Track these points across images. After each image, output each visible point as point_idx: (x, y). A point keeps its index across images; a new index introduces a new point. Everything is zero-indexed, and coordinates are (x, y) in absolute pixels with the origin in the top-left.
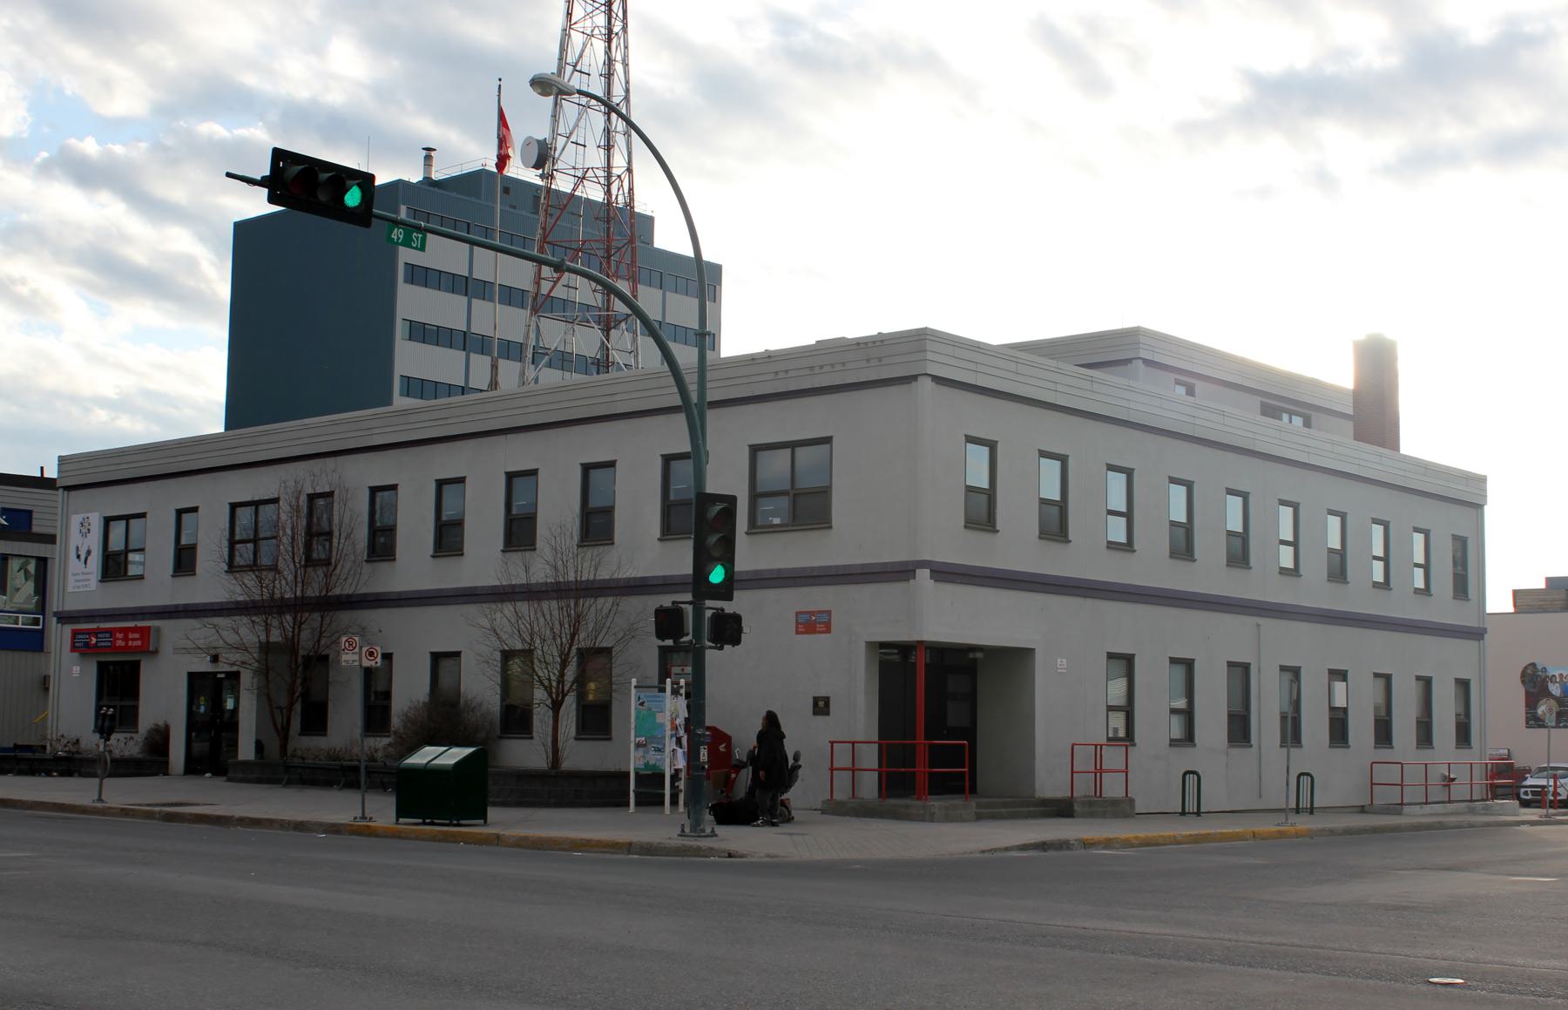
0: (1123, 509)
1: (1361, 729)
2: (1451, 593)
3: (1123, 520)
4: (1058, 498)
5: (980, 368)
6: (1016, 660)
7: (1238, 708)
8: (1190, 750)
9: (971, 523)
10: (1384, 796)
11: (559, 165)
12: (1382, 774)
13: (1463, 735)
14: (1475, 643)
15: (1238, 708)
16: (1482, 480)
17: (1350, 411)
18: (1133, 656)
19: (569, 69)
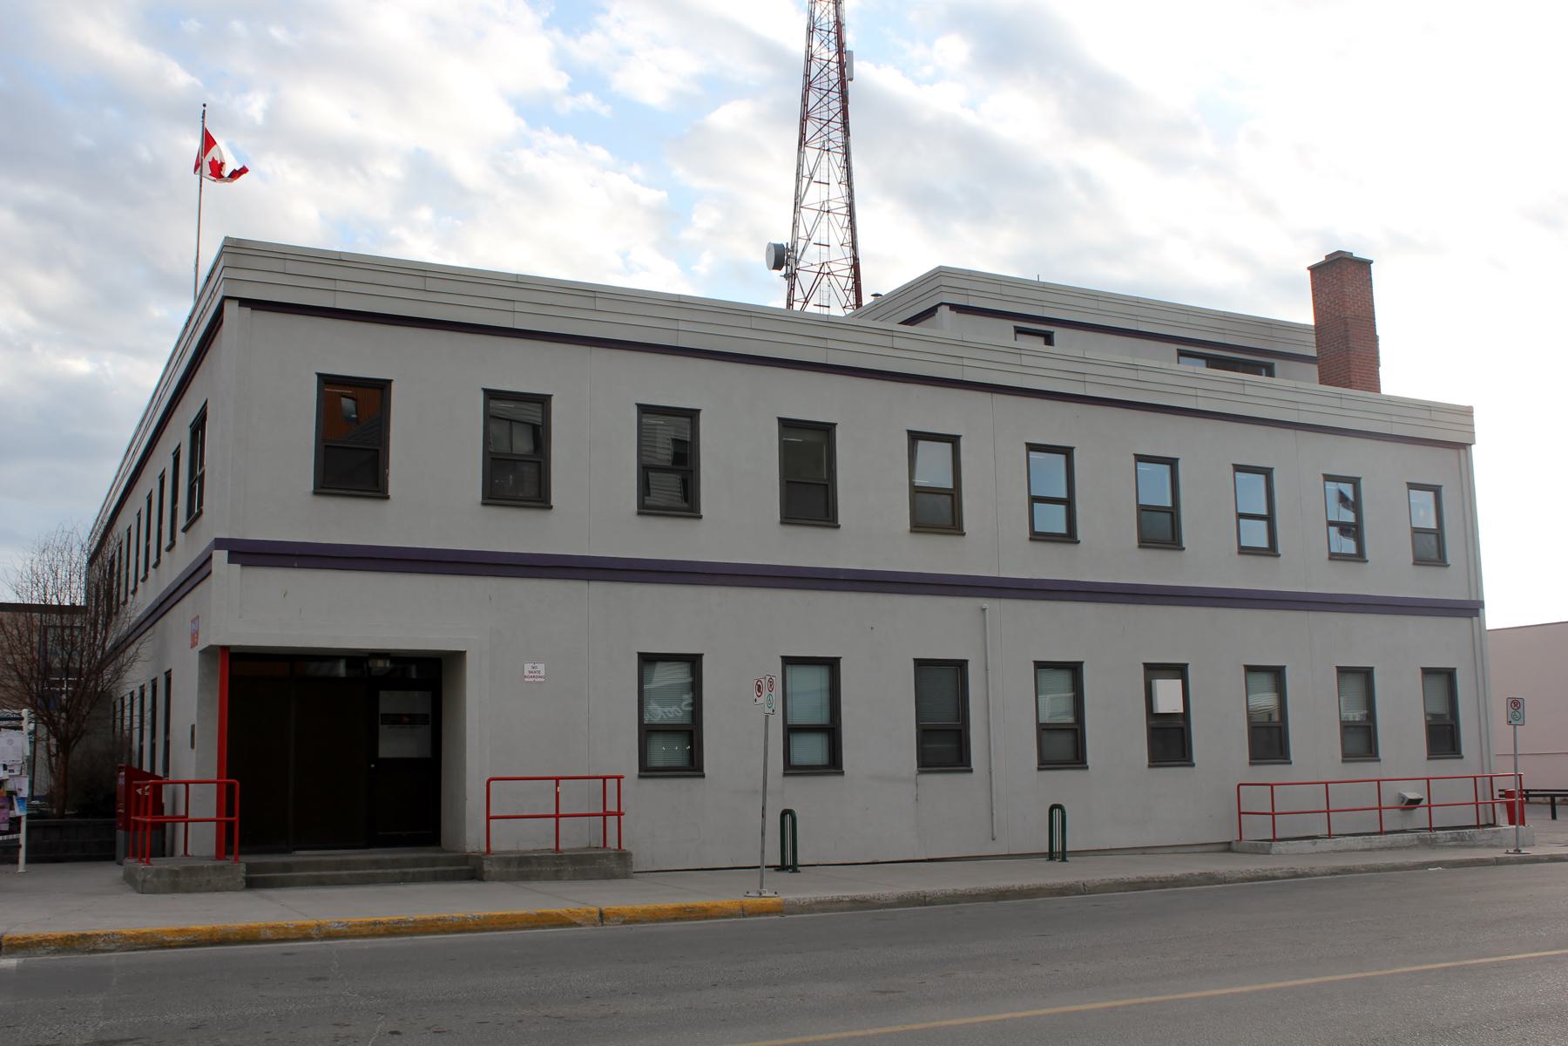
0: (1264, 512)
1: (1220, 737)
2: (309, 483)
3: (1061, 509)
4: (1169, 504)
6: (430, 677)
7: (1440, 708)
8: (837, 779)
9: (1147, 541)
10: (1257, 829)
11: (801, 264)
12: (1256, 799)
13: (1443, 737)
15: (1440, 708)
16: (1467, 412)
17: (1313, 353)
18: (700, 656)
19: (805, 181)
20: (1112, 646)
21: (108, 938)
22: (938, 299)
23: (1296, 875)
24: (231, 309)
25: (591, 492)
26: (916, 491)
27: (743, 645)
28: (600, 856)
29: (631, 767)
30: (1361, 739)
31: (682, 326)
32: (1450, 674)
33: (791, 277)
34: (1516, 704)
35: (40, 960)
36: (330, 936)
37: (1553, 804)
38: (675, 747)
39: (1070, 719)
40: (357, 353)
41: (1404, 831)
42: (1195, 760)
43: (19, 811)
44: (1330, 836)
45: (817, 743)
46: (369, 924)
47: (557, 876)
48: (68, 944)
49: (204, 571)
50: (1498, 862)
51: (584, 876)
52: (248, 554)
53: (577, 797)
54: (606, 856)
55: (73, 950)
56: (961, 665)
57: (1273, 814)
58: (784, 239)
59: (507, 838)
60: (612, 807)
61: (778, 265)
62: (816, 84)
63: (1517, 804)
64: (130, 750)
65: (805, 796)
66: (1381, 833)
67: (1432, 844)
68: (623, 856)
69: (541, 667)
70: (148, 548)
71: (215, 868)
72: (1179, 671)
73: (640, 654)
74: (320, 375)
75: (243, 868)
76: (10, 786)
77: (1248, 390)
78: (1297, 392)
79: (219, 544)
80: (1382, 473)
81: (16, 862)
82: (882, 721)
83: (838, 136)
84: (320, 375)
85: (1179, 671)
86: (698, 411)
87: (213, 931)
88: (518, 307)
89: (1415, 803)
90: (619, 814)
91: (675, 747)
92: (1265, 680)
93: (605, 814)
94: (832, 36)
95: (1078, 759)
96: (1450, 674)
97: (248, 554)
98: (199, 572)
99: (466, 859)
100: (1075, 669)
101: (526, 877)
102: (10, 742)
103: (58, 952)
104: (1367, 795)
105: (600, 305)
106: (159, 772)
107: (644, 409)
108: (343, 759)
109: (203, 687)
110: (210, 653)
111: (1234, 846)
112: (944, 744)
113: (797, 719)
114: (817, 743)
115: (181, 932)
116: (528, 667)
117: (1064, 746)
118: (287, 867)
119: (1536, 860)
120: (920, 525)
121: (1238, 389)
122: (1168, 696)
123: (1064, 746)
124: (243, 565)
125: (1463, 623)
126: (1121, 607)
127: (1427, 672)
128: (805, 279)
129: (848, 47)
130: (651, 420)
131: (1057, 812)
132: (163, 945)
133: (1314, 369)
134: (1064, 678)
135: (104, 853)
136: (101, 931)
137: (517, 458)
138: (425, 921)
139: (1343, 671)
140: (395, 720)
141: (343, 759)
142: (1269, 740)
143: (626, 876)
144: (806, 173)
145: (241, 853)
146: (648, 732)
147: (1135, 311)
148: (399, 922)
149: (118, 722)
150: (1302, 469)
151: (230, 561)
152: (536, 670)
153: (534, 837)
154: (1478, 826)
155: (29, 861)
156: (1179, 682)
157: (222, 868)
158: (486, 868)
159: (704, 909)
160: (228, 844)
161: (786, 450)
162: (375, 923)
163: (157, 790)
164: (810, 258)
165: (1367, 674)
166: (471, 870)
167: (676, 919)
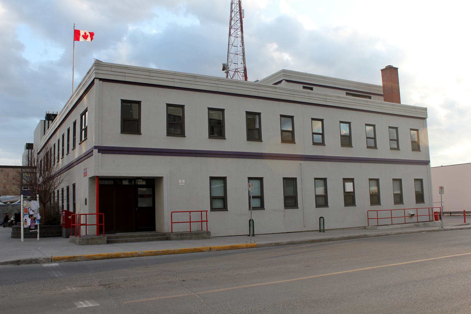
1: (363, 199)
3: (373, 140)
5: (127, 75)
6: (153, 183)
7: (419, 190)
11: (230, 69)
13: (420, 198)
14: (425, 166)
16: (426, 109)
18: (263, 178)
19: (231, 46)
20: (334, 173)
21: (80, 257)
22: (288, 78)
23: (387, 235)
24: (97, 81)
25: (196, 133)
26: (282, 131)
27: (238, 175)
28: (202, 233)
29: (209, 209)
30: (399, 199)
31: (220, 86)
32: (421, 180)
33: (227, 73)
34: (441, 188)
35: (63, 263)
36: (139, 256)
37: (465, 216)
38: (220, 202)
39: (323, 194)
40: (132, 94)
41: (410, 223)
42: (356, 204)
43: (37, 223)
44: (392, 224)
45: (258, 201)
46: (149, 252)
47: (191, 239)
48: (70, 259)
49: (91, 154)
50: (438, 231)
51: (198, 238)
52: (103, 150)
53: (195, 217)
54: (204, 233)
55: (71, 261)
56: (295, 179)
57: (392, 218)
58: (225, 62)
59: (177, 228)
60: (204, 219)
61: (224, 69)
62: (233, 19)
63: (438, 216)
64: (58, 207)
65: (256, 215)
66: (405, 223)
67: (418, 226)
68: (208, 233)
69: (184, 181)
70: (63, 150)
71: (98, 238)
72: (352, 180)
73: (210, 177)
74: (121, 100)
75: (106, 238)
76: (34, 216)
77: (369, 103)
78: (377, 103)
79: (95, 147)
80: (404, 126)
81: (36, 237)
82: (274, 194)
83: (240, 33)
84: (121, 100)
85: (352, 180)
86: (224, 109)
87: (108, 255)
88: (175, 80)
89: (413, 215)
90: (207, 221)
91: (220, 202)
92: (374, 183)
93: (202, 221)
94: (238, 5)
95: (326, 204)
96: (421, 180)
97: (103, 150)
98: (89, 154)
99: (164, 234)
100: (325, 180)
101: (182, 239)
102: (34, 204)
103: (67, 261)
104: (401, 213)
105: (197, 80)
106: (71, 210)
107: (210, 109)
108: (128, 207)
109: (90, 188)
110: (92, 179)
111: (367, 227)
112: (291, 201)
113: (215, 194)
114: (258, 201)
115: (100, 255)
116: (180, 181)
117: (322, 201)
118: (117, 237)
119: (447, 230)
120: (284, 141)
121: (366, 103)
122: (349, 187)
123: (322, 201)
124: (102, 153)
125: (424, 167)
126: (337, 163)
127: (415, 180)
128: (231, 73)
129: (242, 8)
130: (211, 112)
131: (322, 219)
132: (95, 259)
133: (382, 98)
134: (322, 182)
135: (59, 235)
136: (79, 256)
137: (175, 122)
138: (164, 251)
139: (394, 180)
140: (143, 196)
141: (128, 207)
142: (375, 199)
143: (209, 238)
144: (231, 43)
145: (105, 234)
146: (213, 199)
147: (335, 82)
148: (157, 251)
149: (52, 199)
150: (383, 124)
151: (99, 152)
152: (182, 182)
153: (184, 228)
154: (430, 221)
155: (40, 237)
156: (352, 183)
157: (100, 238)
158: (172, 237)
159: (237, 247)
160: (100, 231)
161: (247, 119)
162: (151, 252)
163: (74, 217)
164: (232, 67)
165: (400, 180)
166: (166, 237)
167: (230, 249)
